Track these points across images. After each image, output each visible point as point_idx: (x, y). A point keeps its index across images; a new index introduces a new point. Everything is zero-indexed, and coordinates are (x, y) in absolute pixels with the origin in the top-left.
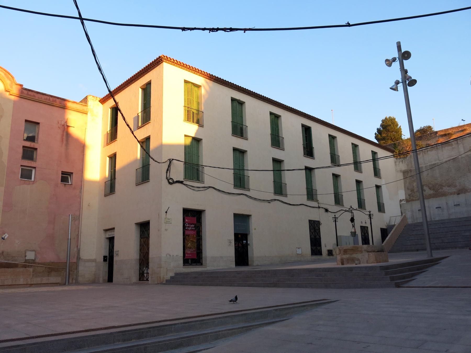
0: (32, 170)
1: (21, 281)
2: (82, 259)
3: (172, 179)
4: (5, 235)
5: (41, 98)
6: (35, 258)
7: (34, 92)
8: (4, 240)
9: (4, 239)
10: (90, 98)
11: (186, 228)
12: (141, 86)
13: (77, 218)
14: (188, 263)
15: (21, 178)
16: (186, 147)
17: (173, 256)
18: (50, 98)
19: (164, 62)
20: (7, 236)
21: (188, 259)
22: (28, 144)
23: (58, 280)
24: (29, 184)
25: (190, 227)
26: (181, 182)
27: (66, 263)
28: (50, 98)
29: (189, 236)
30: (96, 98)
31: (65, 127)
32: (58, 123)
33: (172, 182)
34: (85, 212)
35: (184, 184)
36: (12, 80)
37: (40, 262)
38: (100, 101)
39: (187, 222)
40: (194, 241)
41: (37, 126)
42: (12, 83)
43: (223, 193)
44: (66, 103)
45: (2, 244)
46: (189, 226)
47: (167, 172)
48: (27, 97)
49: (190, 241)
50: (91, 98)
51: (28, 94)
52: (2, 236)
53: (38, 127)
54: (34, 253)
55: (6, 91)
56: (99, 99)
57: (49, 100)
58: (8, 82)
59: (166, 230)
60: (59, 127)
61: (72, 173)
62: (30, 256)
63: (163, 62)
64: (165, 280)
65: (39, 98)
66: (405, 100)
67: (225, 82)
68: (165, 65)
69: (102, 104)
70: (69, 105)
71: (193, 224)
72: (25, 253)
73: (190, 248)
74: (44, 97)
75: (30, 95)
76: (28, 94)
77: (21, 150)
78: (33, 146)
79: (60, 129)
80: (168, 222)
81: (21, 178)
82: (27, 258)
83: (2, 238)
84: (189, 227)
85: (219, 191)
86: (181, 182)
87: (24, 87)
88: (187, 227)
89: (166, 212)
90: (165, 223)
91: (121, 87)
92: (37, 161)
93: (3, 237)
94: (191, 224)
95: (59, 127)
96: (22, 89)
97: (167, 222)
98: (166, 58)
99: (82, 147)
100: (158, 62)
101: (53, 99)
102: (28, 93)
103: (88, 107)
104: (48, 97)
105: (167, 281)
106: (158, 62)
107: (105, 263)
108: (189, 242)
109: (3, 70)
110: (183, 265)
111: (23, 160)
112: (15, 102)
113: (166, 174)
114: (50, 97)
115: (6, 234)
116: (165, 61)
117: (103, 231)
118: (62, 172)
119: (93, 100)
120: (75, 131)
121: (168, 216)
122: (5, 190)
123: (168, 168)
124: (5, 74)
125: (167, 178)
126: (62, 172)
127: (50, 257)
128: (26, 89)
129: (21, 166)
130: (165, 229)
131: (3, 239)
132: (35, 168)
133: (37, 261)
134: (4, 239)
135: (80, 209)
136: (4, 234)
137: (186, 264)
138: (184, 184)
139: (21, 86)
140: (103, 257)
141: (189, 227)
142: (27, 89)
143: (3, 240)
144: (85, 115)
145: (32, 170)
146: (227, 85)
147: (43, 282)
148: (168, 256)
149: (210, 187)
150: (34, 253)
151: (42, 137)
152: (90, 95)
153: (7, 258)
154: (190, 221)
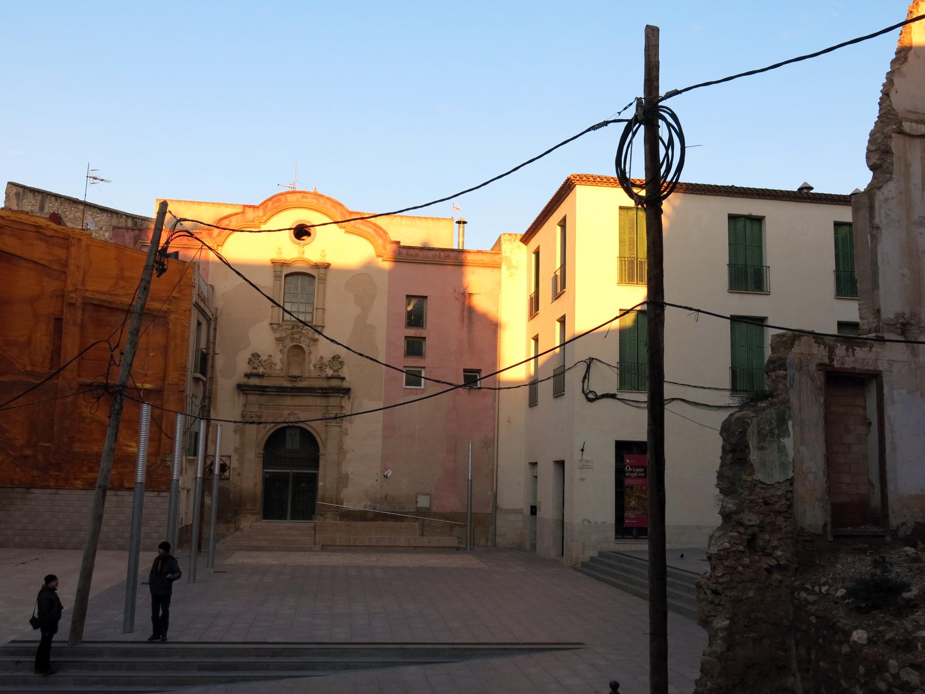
1: (402, 542)
2: (501, 509)
3: (594, 392)
4: (387, 472)
5: (428, 257)
6: (430, 506)
10: (505, 238)
11: (627, 474)
12: (559, 223)
13: (490, 443)
14: (631, 534)
15: (406, 385)
16: (622, 332)
17: (596, 523)
18: (440, 253)
19: (577, 186)
20: (391, 472)
21: (632, 528)
22: (412, 332)
23: (454, 542)
25: (634, 472)
26: (613, 396)
27: (467, 513)
28: (440, 253)
29: (632, 487)
30: (514, 237)
31: (465, 296)
32: (455, 291)
33: (594, 397)
34: (504, 432)
35: (619, 399)
36: (385, 238)
37: (438, 511)
38: (521, 240)
39: (628, 464)
40: (644, 496)
42: (385, 242)
43: (704, 407)
44: (464, 258)
46: (632, 470)
47: (583, 382)
48: (407, 259)
49: (636, 496)
50: (507, 237)
51: (408, 254)
54: (427, 498)
56: (519, 237)
57: (440, 256)
58: (380, 241)
59: (582, 480)
60: (456, 298)
61: (481, 370)
62: (423, 502)
63: (575, 185)
64: (580, 562)
66: (733, 346)
67: (710, 188)
68: (580, 191)
69: (526, 245)
70: (470, 257)
71: (642, 467)
72: (417, 497)
73: (635, 509)
74: (431, 254)
75: (411, 255)
77: (402, 344)
79: (458, 300)
80: (585, 466)
81: (406, 385)
82: (419, 505)
84: (631, 472)
85: (695, 404)
86: (613, 396)
87: (401, 244)
88: (628, 472)
89: (582, 450)
91: (545, 213)
94: (638, 467)
95: (456, 298)
97: (584, 467)
98: (578, 178)
99: (493, 327)
100: (567, 188)
101: (445, 254)
102: (408, 252)
103: (503, 254)
104: (438, 253)
105: (583, 564)
106: (567, 188)
108: (633, 498)
109: (371, 225)
110: (616, 538)
111: (406, 359)
112: (391, 272)
113: (582, 384)
115: (389, 470)
116: (578, 183)
117: (528, 464)
118: (464, 369)
119: (510, 240)
120: (481, 302)
121: (586, 456)
123: (586, 374)
124: (375, 231)
125: (583, 392)
126: (464, 369)
127: (452, 504)
128: (405, 247)
130: (581, 479)
131: (386, 477)
132: (424, 368)
133: (434, 509)
135: (495, 428)
136: (387, 470)
137: (626, 537)
138: (619, 399)
140: (529, 508)
141: (631, 472)
143: (385, 478)
144: (496, 270)
145: (421, 371)
146: (717, 192)
147: (431, 545)
148: (586, 523)
149: (673, 399)
150: (427, 498)
151: (431, 316)
152: (504, 234)
153: (393, 504)
154: (634, 461)
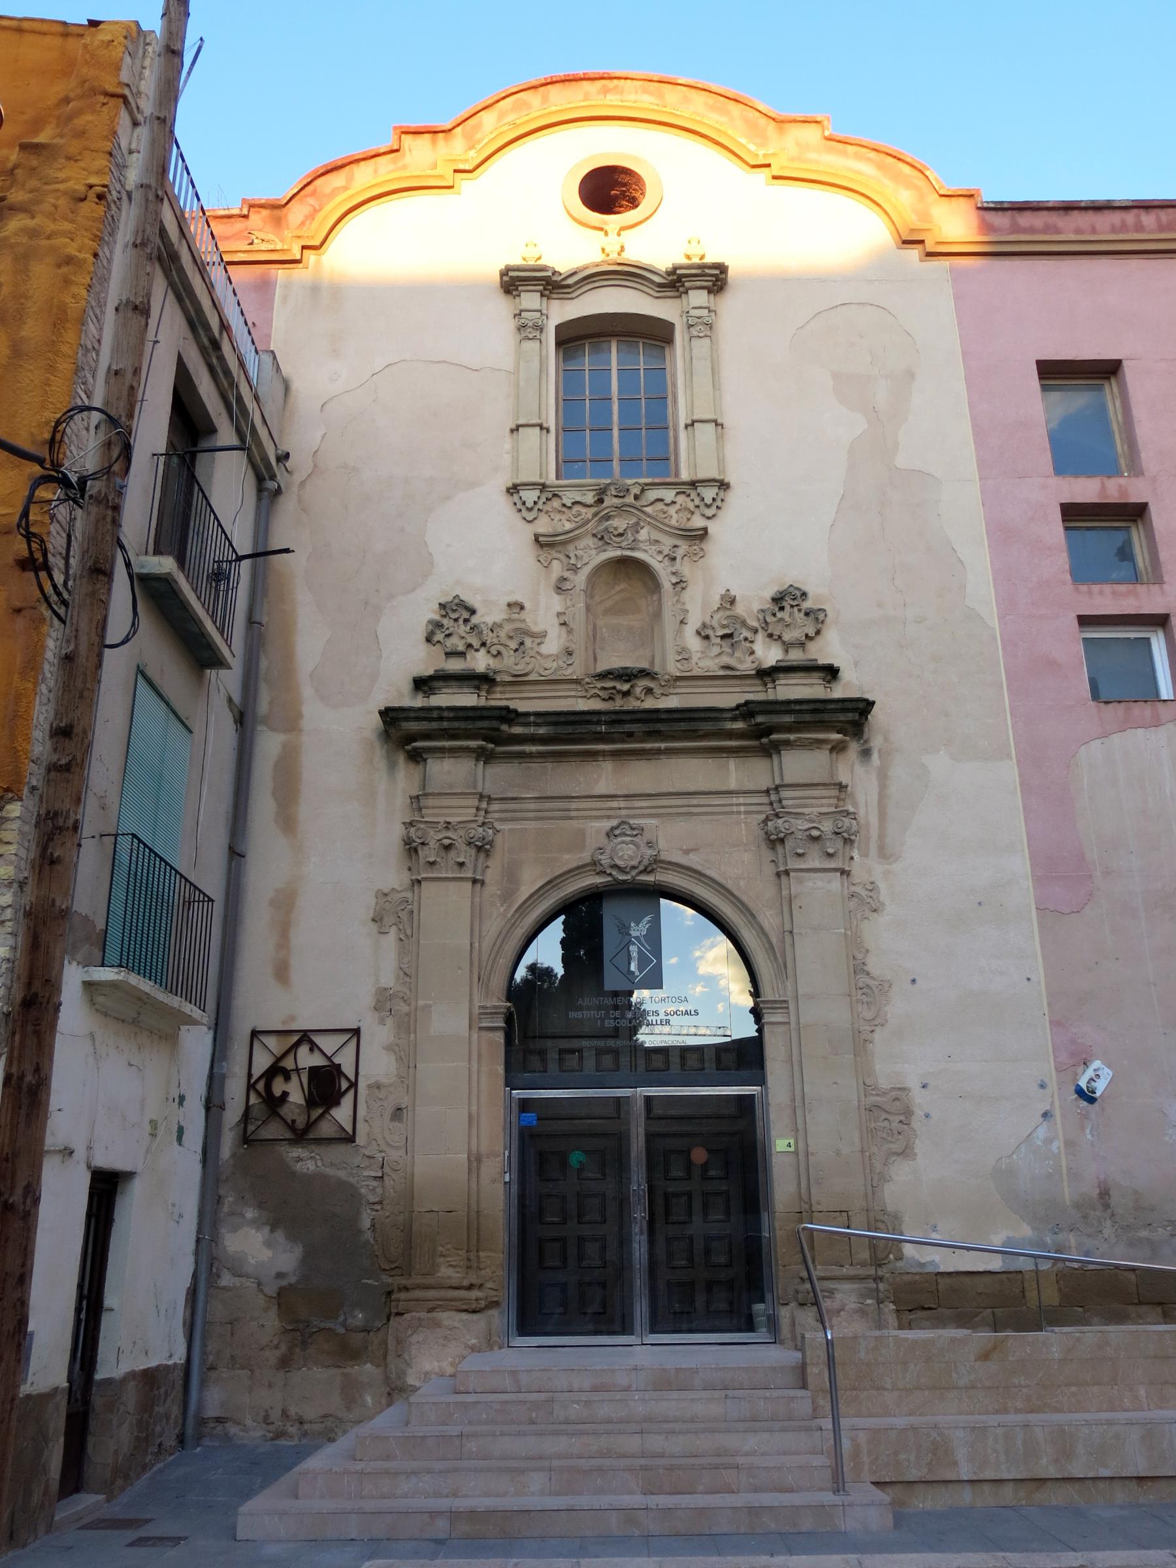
0: (1148, 639)
4: (1090, 1073)
7: (1045, 213)
8: (1096, 1105)
9: (1091, 1100)
20: (1107, 1074)
24: (1157, 723)
41: (1110, 390)
45: (1088, 1131)
52: (1076, 1077)
53: (1115, 389)
55: (905, 242)
57: (1139, 228)
65: (1078, 231)
75: (1032, 230)
76: (1016, 229)
78: (1116, 494)
83: (1080, 1092)
90: (470, 844)
92: (1166, 578)
93: (1083, 1084)
96: (982, 212)
101: (1158, 220)
104: (1130, 217)
107: (407, 686)
114: (1135, 211)
115: (1097, 1064)
122: (1020, 776)
124: (880, 167)
129: (1085, 621)
131: (1086, 1096)
134: (1091, 1100)
139: (971, 196)
142: (1006, 206)
153: (1143, 1234)
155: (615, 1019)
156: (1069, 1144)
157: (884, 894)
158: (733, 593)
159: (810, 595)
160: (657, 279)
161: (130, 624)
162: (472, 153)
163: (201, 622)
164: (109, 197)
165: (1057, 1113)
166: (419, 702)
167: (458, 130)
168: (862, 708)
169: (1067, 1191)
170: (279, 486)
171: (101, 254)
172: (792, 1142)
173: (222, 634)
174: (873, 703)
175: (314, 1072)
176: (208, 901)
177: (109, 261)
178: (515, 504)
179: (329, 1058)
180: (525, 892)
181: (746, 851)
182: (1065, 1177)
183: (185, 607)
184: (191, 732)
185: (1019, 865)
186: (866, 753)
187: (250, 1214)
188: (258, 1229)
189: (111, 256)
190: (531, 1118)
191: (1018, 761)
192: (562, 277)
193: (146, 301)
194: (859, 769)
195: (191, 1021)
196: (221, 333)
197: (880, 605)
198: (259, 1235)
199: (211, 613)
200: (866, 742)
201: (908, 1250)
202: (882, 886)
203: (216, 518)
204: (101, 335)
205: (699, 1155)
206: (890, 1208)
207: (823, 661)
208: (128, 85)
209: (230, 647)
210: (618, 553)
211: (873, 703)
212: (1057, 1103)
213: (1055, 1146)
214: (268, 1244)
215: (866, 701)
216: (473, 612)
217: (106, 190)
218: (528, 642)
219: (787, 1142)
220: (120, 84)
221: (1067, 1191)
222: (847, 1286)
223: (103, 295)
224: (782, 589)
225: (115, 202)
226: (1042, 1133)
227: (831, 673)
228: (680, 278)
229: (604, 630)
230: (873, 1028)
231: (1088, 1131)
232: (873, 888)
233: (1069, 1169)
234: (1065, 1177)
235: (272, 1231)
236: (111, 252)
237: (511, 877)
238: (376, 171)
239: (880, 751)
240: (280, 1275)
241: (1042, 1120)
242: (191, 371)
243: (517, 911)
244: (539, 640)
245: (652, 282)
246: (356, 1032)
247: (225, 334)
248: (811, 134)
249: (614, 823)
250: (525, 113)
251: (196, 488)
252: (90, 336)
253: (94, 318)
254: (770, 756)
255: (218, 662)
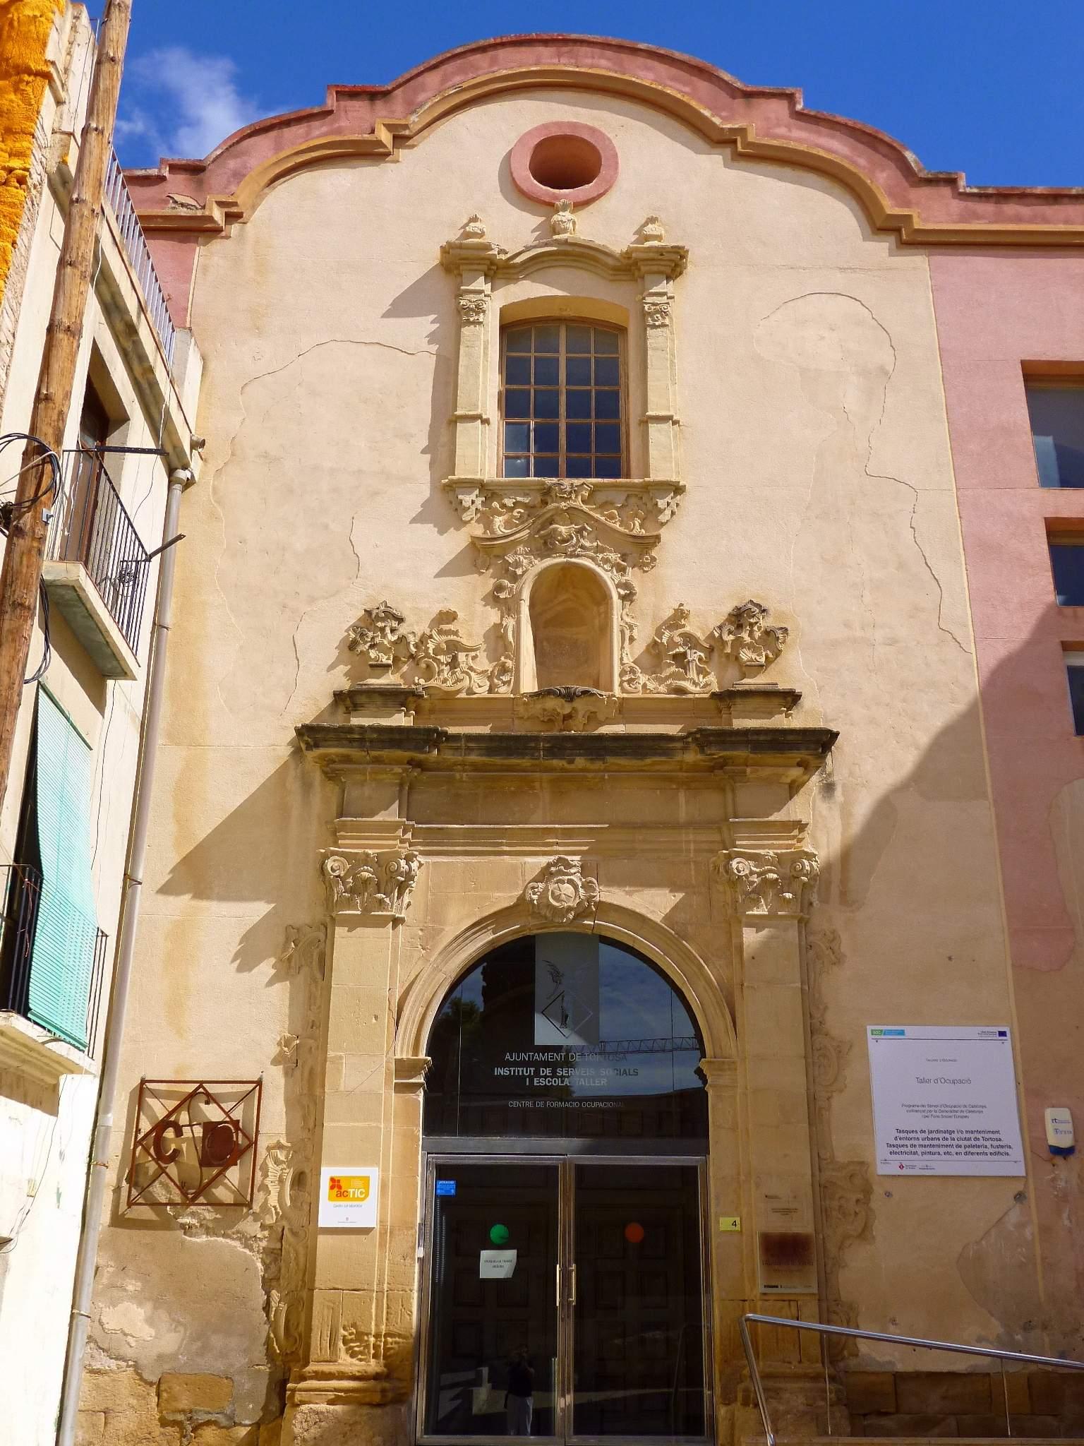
45: (1065, 1215)
55: (878, 229)
155: (546, 1077)
156: (1045, 1230)
157: (845, 946)
158: (685, 608)
159: (771, 611)
160: (610, 261)
161: (42, 657)
162: (414, 118)
163: (107, 631)
164: (30, 182)
165: (1032, 1195)
166: (338, 721)
167: (398, 92)
168: (822, 741)
169: (1041, 1284)
170: (193, 476)
171: (19, 241)
172: (738, 1220)
173: (126, 637)
174: (837, 734)
175: (210, 1127)
176: (102, 936)
177: (28, 249)
178: (451, 503)
179: (227, 1114)
180: (451, 931)
181: (695, 893)
182: (1039, 1268)
183: (90, 615)
184: (91, 749)
185: (993, 916)
186: (829, 788)
187: (132, 1286)
188: (140, 1304)
189: (29, 243)
190: (449, 1187)
191: (995, 801)
192: (508, 256)
193: (79, 322)
194: (823, 807)
195: (73, 1069)
196: (139, 317)
197: (847, 625)
198: (141, 1311)
199: (117, 620)
200: (830, 775)
201: (864, 1347)
202: (845, 937)
203: (123, 509)
204: (15, 328)
205: (635, 1232)
206: (844, 1296)
207: (782, 686)
208: (53, 63)
209: (135, 655)
210: (562, 560)
211: (837, 734)
212: (1031, 1187)
213: (1028, 1232)
214: (150, 1321)
215: (830, 732)
216: (400, 620)
217: (27, 173)
218: (462, 657)
219: (731, 1220)
220: (46, 62)
221: (1041, 1284)
222: (796, 1385)
223: (19, 285)
224: (739, 605)
225: (35, 187)
226: (1014, 1217)
227: (791, 699)
228: (636, 263)
229: (545, 644)
230: (829, 1094)
231: (1065, 1215)
232: (834, 938)
233: (1044, 1259)
234: (1039, 1268)
235: (155, 1308)
236: (30, 240)
237: (435, 913)
238: (308, 134)
239: (844, 786)
240: (160, 1357)
241: (1012, 1202)
242: (105, 358)
243: (440, 953)
244: (473, 654)
245: (605, 265)
246: (259, 1083)
247: (143, 316)
248: (778, 108)
249: (552, 859)
250: (471, 75)
251: (119, 507)
252: (5, 330)
253: (10, 311)
254: (723, 790)
255: (122, 672)
